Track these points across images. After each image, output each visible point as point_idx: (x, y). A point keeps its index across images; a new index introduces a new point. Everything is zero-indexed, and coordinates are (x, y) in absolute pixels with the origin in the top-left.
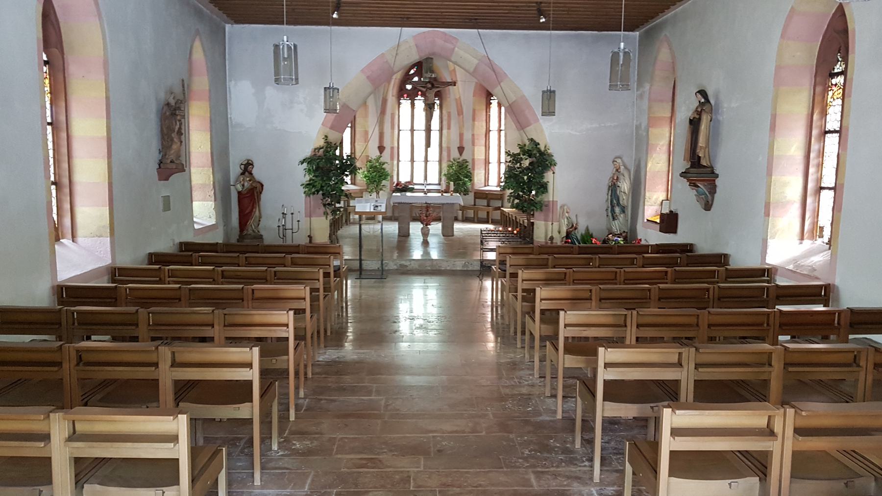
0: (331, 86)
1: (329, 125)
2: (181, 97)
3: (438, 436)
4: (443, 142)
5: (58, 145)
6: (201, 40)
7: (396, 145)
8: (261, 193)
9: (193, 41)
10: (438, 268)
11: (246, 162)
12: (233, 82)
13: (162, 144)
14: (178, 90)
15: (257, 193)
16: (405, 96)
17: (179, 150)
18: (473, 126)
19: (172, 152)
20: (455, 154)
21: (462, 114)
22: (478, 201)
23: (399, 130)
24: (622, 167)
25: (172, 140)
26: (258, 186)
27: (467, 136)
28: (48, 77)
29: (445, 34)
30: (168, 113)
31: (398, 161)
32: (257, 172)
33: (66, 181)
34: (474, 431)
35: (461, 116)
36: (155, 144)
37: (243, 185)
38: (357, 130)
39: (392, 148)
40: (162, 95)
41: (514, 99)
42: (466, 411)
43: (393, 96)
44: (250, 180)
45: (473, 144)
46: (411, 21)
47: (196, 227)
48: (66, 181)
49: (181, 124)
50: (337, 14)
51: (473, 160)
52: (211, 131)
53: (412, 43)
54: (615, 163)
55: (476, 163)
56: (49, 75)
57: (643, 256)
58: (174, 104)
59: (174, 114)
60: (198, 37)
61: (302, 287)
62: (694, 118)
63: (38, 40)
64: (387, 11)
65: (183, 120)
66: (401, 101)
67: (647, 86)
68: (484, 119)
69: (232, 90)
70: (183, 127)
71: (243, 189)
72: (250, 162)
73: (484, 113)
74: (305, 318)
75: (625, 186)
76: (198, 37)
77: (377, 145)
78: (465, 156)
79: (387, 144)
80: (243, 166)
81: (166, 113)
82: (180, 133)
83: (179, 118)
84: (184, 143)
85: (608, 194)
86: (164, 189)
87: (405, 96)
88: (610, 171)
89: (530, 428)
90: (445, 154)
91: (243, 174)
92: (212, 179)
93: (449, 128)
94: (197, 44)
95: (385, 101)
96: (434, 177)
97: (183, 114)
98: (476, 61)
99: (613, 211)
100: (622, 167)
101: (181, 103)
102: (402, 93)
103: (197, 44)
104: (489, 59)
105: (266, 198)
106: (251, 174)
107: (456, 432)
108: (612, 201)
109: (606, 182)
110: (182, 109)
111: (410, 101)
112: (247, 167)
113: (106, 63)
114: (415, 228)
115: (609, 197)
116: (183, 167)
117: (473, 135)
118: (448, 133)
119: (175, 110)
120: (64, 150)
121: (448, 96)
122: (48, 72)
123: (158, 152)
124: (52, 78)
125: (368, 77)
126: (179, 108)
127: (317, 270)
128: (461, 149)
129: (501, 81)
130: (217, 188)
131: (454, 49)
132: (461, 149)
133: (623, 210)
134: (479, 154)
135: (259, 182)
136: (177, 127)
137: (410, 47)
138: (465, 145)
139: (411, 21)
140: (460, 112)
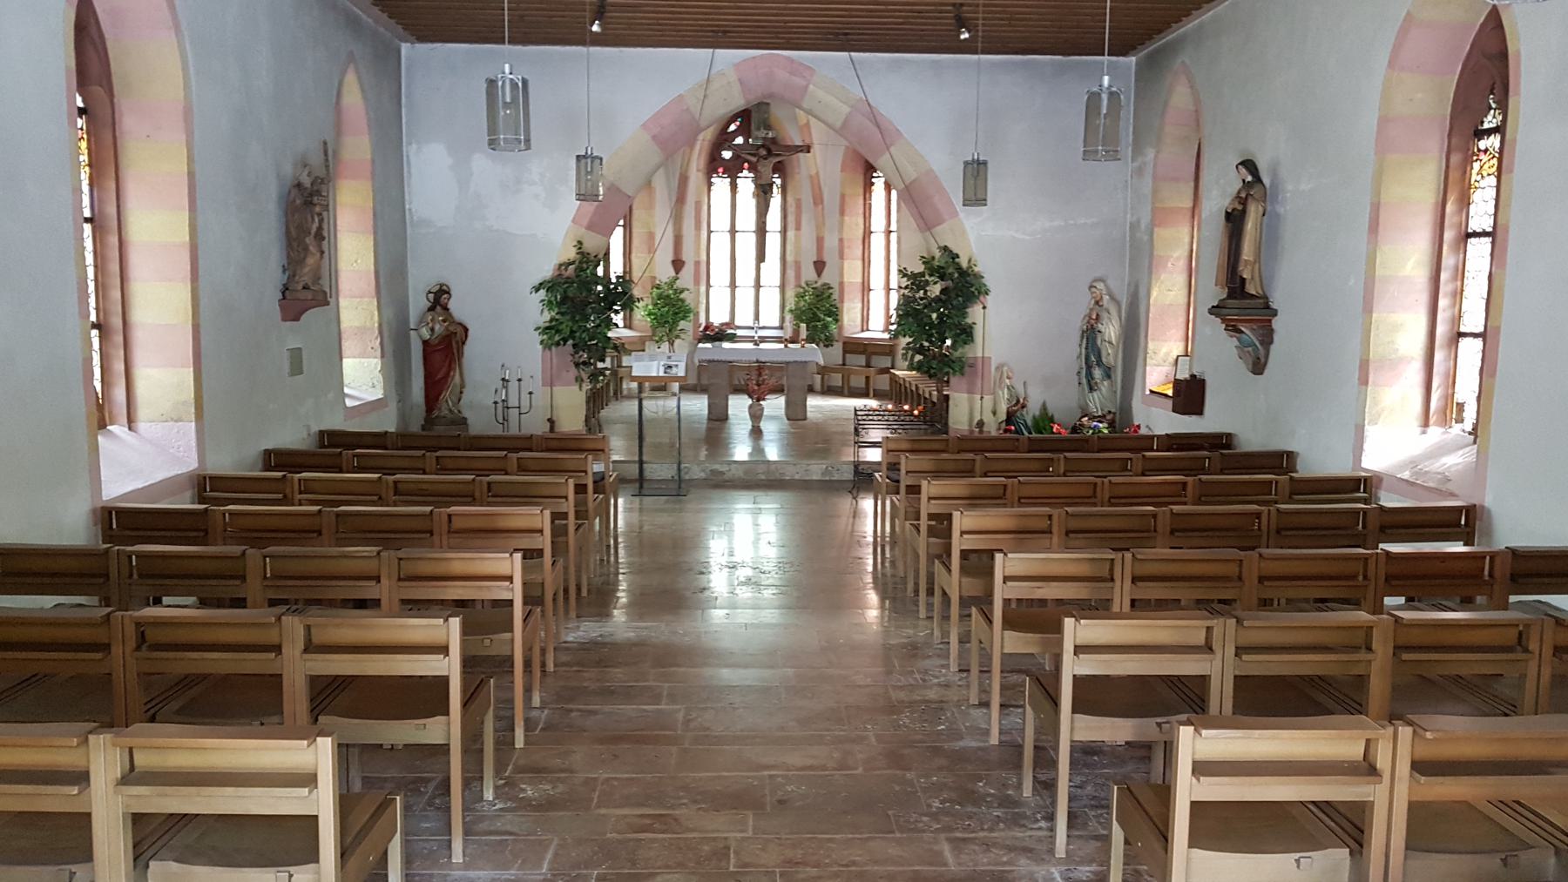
0: (589, 153)
1: (585, 222)
2: (321, 173)
3: (778, 776)
4: (788, 252)
5: (104, 258)
6: (357, 71)
7: (704, 257)
8: (464, 343)
9: (343, 73)
10: (778, 477)
11: (438, 288)
12: (414, 146)
13: (288, 256)
14: (316, 160)
15: (457, 342)
16: (721, 170)
17: (318, 267)
18: (841, 224)
19: (306, 270)
20: (809, 273)
21: (822, 202)
22: (850, 358)
23: (710, 232)
24: (1106, 298)
25: (306, 249)
26: (459, 330)
27: (831, 242)
28: (85, 136)
29: (791, 60)
30: (298, 202)
31: (708, 286)
32: (456, 306)
33: (117, 321)
34: (842, 766)
35: (820, 207)
36: (275, 256)
37: (432, 330)
38: (635, 230)
39: (697, 264)
40: (288, 169)
41: (914, 175)
42: (828, 730)
43: (698, 170)
44: (444, 321)
45: (841, 257)
46: (730, 37)
47: (349, 403)
48: (117, 321)
49: (321, 221)
50: (600, 25)
51: (841, 284)
52: (375, 233)
53: (733, 77)
54: (1094, 290)
55: (846, 289)
56: (88, 133)
57: (1144, 456)
58: (309, 186)
59: (309, 204)
60: (352, 66)
61: (536, 510)
62: (1234, 210)
63: (68, 71)
64: (688, 19)
65: (325, 214)
66: (713, 180)
67: (1150, 154)
68: (861, 211)
69: (413, 160)
70: (325, 226)
71: (431, 335)
72: (445, 288)
73: (861, 201)
74: (541, 565)
75: (1111, 330)
76: (352, 66)
77: (670, 257)
78: (827, 277)
79: (688, 255)
80: (431, 296)
81: (294, 201)
82: (319, 237)
83: (317, 209)
84: (326, 254)
85: (1080, 345)
86: (292, 336)
87: (721, 170)
88: (1084, 303)
89: (943, 762)
90: (791, 273)
91: (431, 309)
92: (376, 318)
93: (798, 228)
94: (351, 79)
95: (684, 180)
96: (771, 314)
97: (325, 203)
98: (846, 109)
99: (1090, 375)
100: (1106, 298)
101: (321, 183)
102: (714, 165)
103: (351, 79)
104: (869, 104)
105: (474, 351)
106: (446, 309)
107: (811, 768)
108: (1087, 358)
109: (1077, 324)
110: (324, 194)
111: (729, 180)
112: (440, 298)
113: (188, 113)
114: (739, 406)
115: (1083, 350)
116: (326, 297)
117: (841, 240)
118: (797, 237)
119: (311, 195)
120: (114, 267)
121: (797, 171)
122: (84, 128)
123: (281, 270)
124: (93, 139)
125: (654, 137)
126: (318, 193)
127: (564, 481)
128: (819, 266)
129: (891, 145)
130: (386, 335)
131: (806, 87)
132: (819, 266)
133: (1108, 373)
134: (852, 273)
135: (460, 324)
136: (315, 225)
137: (729, 83)
138: (826, 258)
139: (730, 37)
140: (818, 200)
